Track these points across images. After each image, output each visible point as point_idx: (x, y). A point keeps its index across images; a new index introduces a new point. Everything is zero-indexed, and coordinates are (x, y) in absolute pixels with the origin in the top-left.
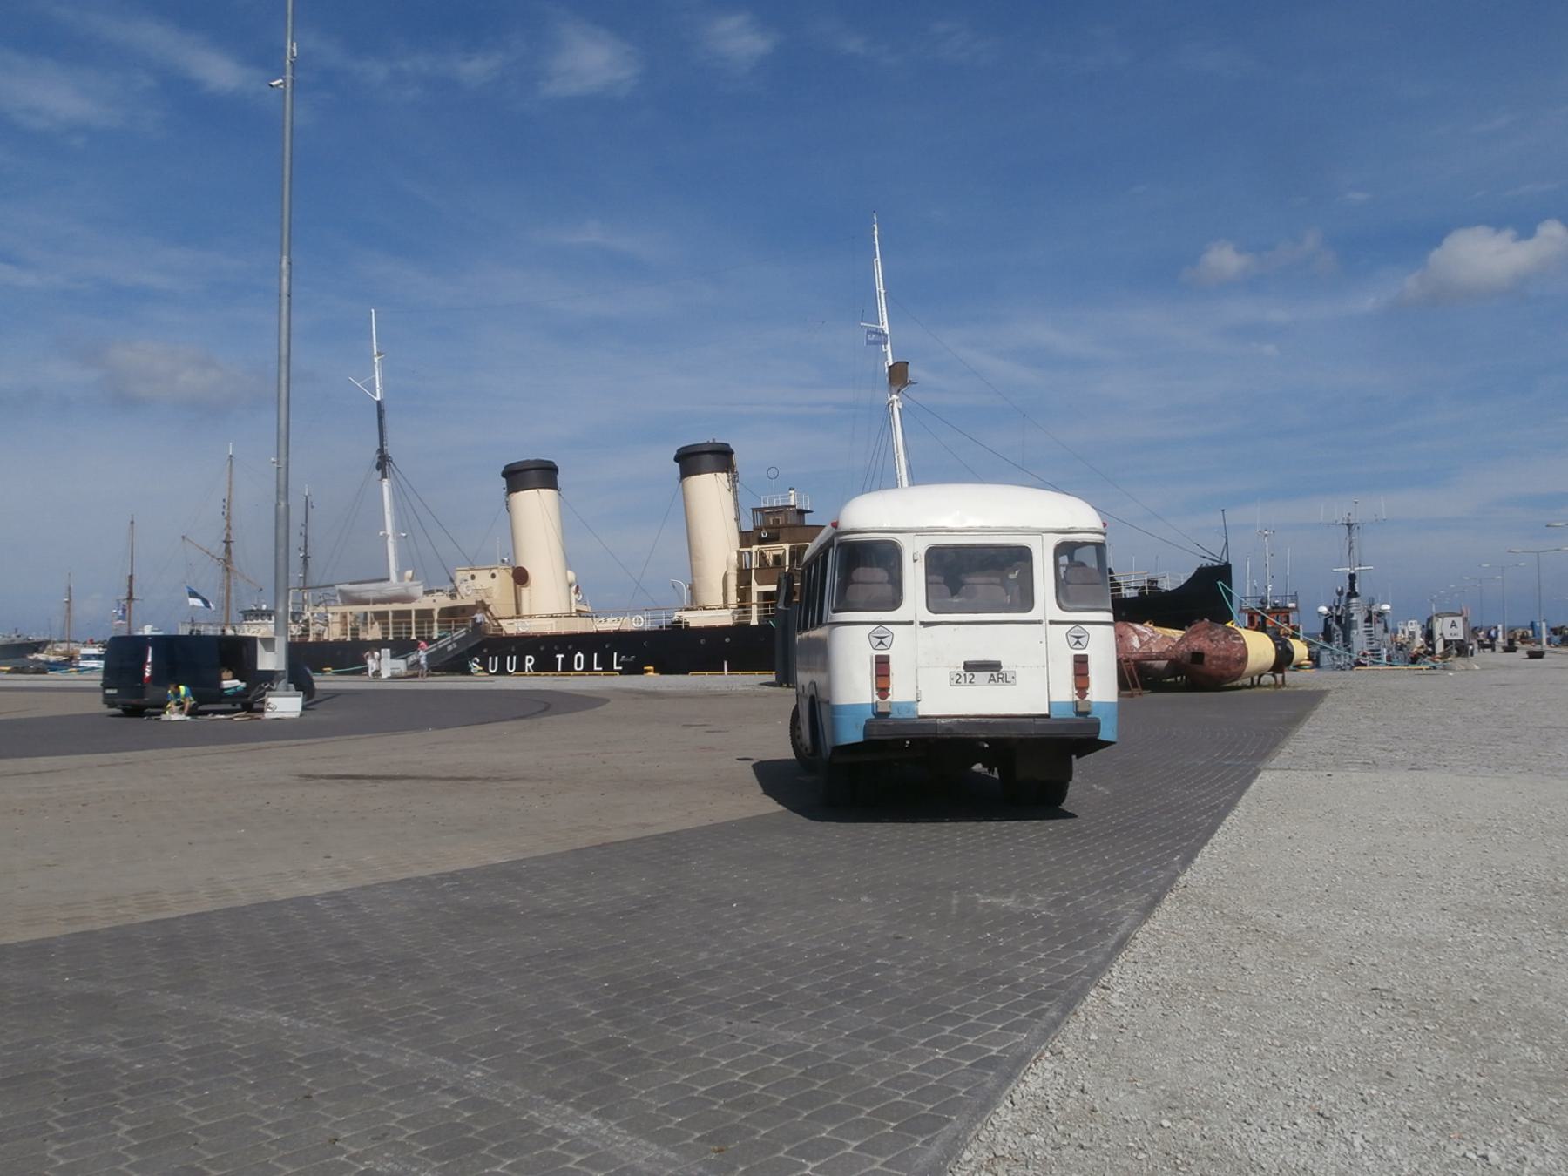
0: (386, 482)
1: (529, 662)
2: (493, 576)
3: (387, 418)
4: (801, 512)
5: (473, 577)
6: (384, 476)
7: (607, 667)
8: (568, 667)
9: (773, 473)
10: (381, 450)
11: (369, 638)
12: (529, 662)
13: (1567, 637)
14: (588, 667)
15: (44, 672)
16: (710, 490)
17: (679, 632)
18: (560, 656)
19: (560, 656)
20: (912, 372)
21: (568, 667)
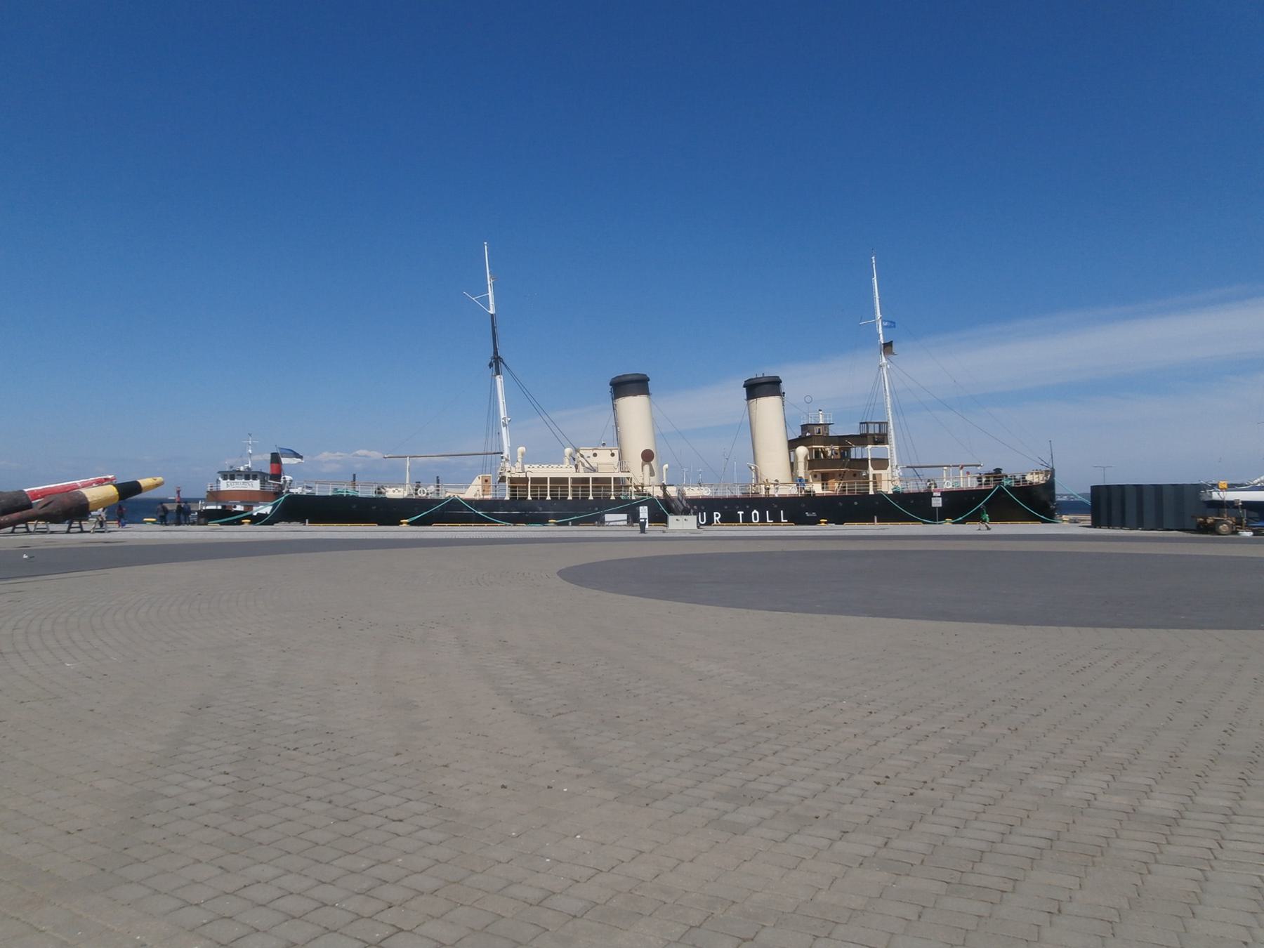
0: (499, 379)
1: (717, 516)
2: (613, 455)
3: (498, 324)
4: (826, 425)
5: (595, 455)
6: (498, 373)
7: (776, 520)
8: (747, 519)
9: (808, 399)
10: (496, 352)
11: (887, 488)
12: (717, 516)
13: (10, 510)
14: (763, 520)
15: (232, 478)
16: (768, 406)
17: (454, 504)
18: (741, 513)
19: (741, 513)
20: (895, 348)
21: (747, 519)
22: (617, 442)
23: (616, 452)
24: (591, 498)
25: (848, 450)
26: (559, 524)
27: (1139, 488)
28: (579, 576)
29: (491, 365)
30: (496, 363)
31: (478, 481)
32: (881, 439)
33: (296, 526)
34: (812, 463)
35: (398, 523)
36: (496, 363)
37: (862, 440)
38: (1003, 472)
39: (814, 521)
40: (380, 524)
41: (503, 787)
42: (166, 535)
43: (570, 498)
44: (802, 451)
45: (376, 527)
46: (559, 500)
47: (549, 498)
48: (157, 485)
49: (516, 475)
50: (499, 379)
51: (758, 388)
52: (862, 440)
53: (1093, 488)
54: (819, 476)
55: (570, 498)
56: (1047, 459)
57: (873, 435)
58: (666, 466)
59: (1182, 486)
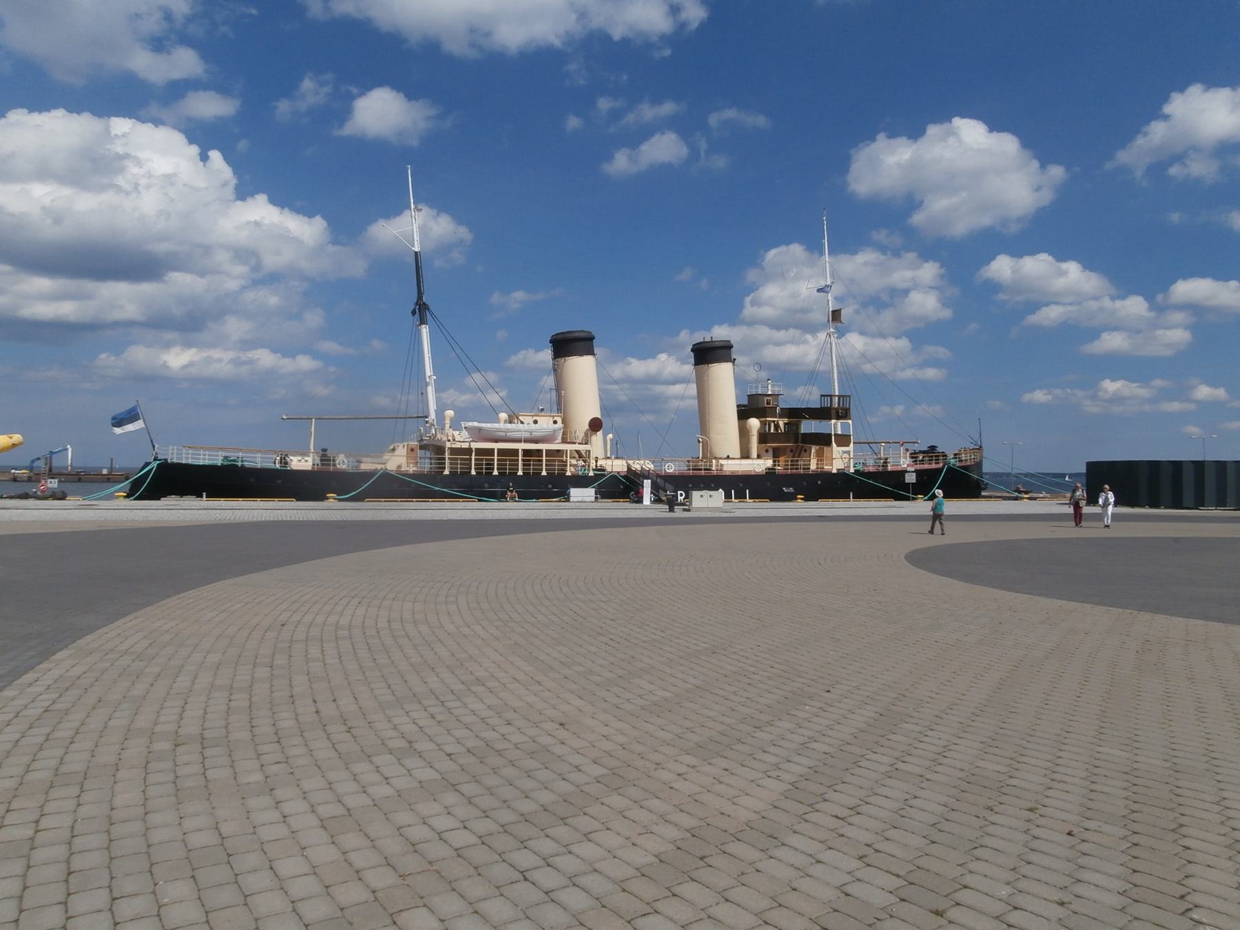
0: (425, 330)
2: (555, 422)
4: (775, 396)
5: (536, 422)
6: (423, 322)
17: (386, 477)
22: (561, 405)
23: (559, 420)
24: (544, 473)
25: (798, 425)
26: (340, 500)
27: (1177, 466)
28: (919, 559)
29: (414, 313)
30: (421, 311)
31: (402, 451)
32: (843, 414)
33: (190, 502)
34: (764, 438)
35: (322, 498)
36: (421, 311)
37: (823, 413)
38: (939, 450)
39: (791, 498)
40: (772, 500)
41: (1069, 834)
42: (90, 515)
43: (520, 473)
44: (754, 423)
45: (294, 504)
46: (508, 477)
47: (496, 473)
48: (14, 445)
49: (458, 445)
50: (425, 330)
51: (706, 354)
52: (823, 413)
53: (1090, 465)
54: (771, 452)
55: (520, 473)
56: (976, 438)
57: (837, 410)
58: (610, 436)
59: (1225, 462)
